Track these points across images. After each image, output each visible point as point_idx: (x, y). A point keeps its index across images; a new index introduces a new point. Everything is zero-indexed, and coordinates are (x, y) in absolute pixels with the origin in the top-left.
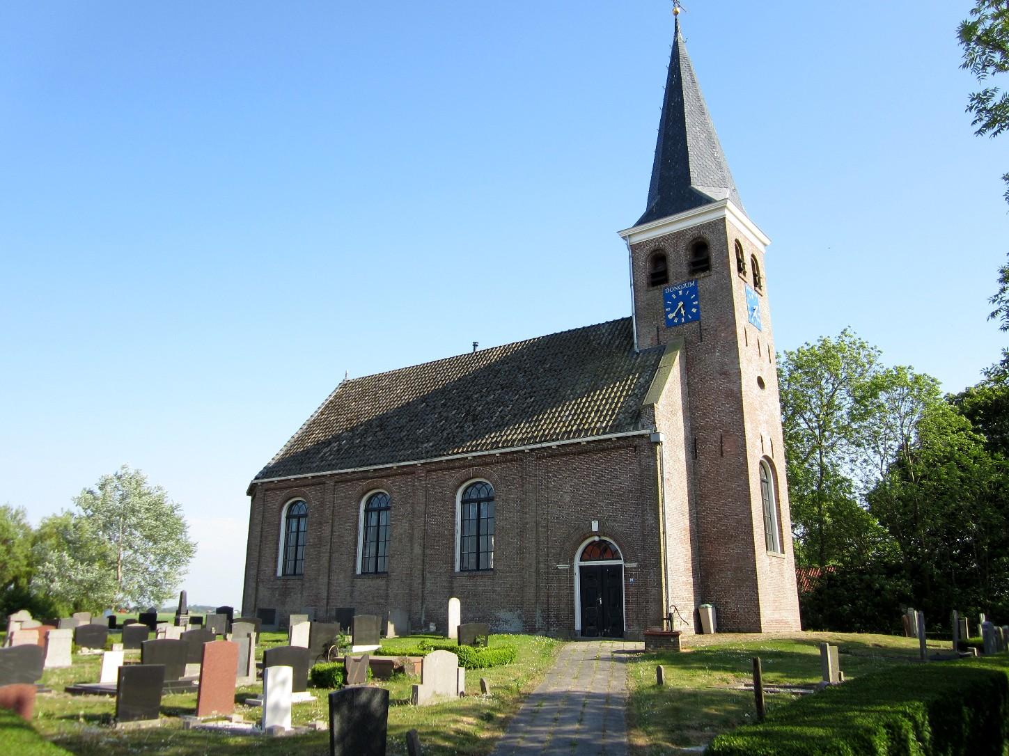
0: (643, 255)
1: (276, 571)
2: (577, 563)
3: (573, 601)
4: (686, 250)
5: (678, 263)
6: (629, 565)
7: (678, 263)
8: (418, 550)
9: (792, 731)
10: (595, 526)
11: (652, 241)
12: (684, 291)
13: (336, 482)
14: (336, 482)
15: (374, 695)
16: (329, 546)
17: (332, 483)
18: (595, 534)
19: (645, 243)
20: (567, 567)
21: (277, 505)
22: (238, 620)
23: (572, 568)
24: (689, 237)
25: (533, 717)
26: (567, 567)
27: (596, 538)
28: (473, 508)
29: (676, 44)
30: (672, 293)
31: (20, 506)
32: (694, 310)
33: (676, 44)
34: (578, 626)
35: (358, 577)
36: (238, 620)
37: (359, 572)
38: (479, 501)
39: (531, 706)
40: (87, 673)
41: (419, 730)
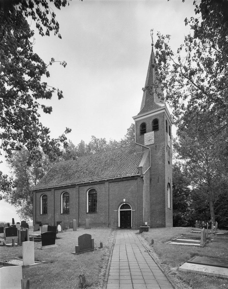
0: (139, 124)
1: (40, 213)
2: (119, 210)
3: (118, 218)
4: (152, 122)
5: (149, 125)
6: (133, 210)
10: (124, 200)
11: (142, 120)
13: (55, 190)
14: (55, 190)
17: (54, 190)
18: (124, 202)
20: (117, 211)
21: (39, 197)
22: (60, 232)
23: (118, 211)
24: (153, 118)
25: (24, 287)
26: (117, 211)
27: (125, 203)
34: (119, 226)
35: (62, 214)
36: (60, 232)
37: (62, 213)
41: (144, 239)
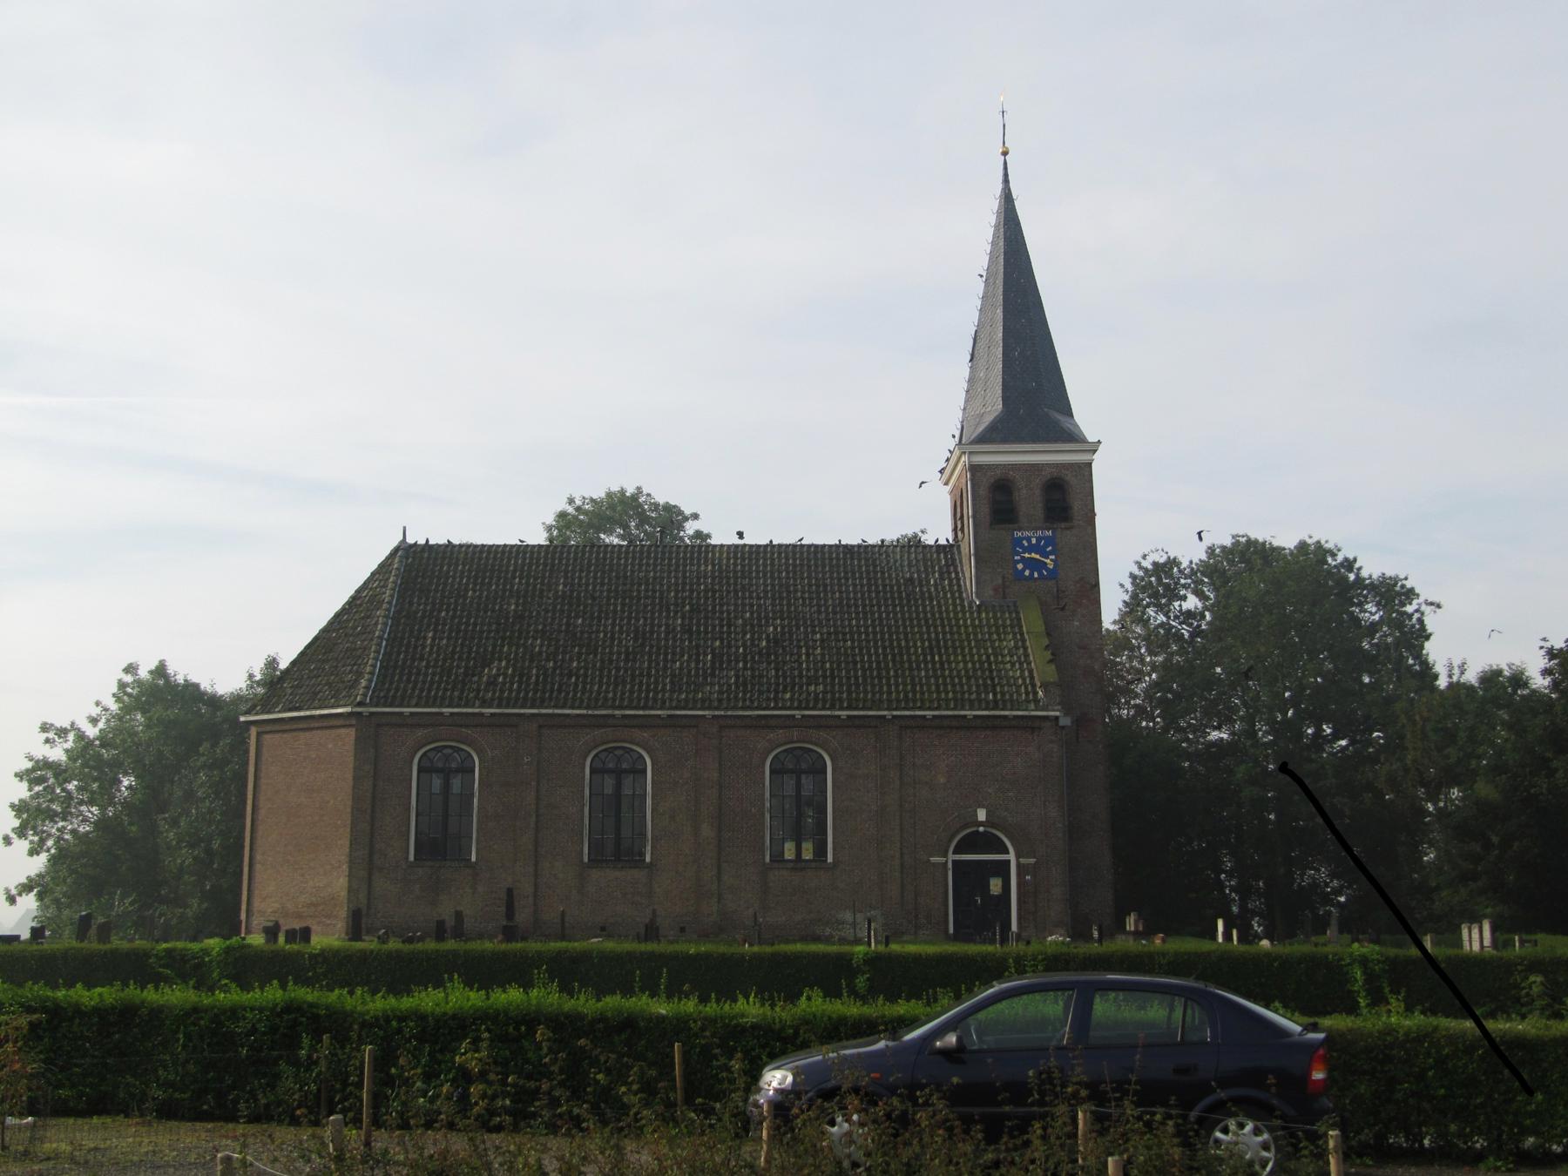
5: (1029, 501)
7: (1029, 501)
8: (707, 831)
9: (566, 989)
12: (1039, 539)
13: (540, 727)
15: (184, 978)
16: (533, 819)
18: (981, 824)
19: (990, 467)
28: (789, 783)
29: (1008, 199)
30: (1022, 539)
31: (695, 516)
32: (1027, 573)
33: (1008, 199)
34: (951, 930)
38: (798, 773)
39: (864, 1029)
40: (1037, 1142)
